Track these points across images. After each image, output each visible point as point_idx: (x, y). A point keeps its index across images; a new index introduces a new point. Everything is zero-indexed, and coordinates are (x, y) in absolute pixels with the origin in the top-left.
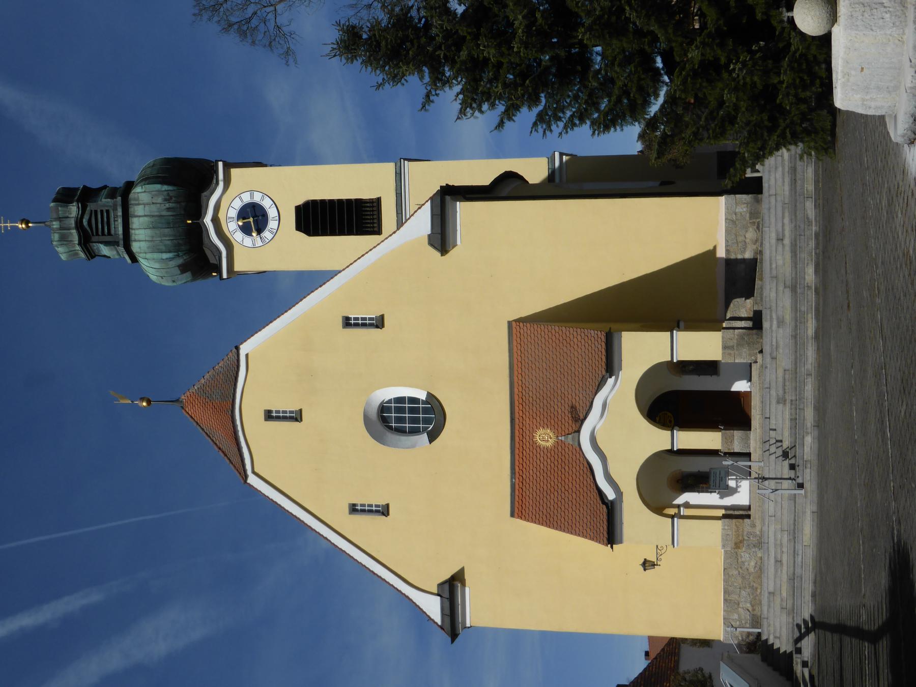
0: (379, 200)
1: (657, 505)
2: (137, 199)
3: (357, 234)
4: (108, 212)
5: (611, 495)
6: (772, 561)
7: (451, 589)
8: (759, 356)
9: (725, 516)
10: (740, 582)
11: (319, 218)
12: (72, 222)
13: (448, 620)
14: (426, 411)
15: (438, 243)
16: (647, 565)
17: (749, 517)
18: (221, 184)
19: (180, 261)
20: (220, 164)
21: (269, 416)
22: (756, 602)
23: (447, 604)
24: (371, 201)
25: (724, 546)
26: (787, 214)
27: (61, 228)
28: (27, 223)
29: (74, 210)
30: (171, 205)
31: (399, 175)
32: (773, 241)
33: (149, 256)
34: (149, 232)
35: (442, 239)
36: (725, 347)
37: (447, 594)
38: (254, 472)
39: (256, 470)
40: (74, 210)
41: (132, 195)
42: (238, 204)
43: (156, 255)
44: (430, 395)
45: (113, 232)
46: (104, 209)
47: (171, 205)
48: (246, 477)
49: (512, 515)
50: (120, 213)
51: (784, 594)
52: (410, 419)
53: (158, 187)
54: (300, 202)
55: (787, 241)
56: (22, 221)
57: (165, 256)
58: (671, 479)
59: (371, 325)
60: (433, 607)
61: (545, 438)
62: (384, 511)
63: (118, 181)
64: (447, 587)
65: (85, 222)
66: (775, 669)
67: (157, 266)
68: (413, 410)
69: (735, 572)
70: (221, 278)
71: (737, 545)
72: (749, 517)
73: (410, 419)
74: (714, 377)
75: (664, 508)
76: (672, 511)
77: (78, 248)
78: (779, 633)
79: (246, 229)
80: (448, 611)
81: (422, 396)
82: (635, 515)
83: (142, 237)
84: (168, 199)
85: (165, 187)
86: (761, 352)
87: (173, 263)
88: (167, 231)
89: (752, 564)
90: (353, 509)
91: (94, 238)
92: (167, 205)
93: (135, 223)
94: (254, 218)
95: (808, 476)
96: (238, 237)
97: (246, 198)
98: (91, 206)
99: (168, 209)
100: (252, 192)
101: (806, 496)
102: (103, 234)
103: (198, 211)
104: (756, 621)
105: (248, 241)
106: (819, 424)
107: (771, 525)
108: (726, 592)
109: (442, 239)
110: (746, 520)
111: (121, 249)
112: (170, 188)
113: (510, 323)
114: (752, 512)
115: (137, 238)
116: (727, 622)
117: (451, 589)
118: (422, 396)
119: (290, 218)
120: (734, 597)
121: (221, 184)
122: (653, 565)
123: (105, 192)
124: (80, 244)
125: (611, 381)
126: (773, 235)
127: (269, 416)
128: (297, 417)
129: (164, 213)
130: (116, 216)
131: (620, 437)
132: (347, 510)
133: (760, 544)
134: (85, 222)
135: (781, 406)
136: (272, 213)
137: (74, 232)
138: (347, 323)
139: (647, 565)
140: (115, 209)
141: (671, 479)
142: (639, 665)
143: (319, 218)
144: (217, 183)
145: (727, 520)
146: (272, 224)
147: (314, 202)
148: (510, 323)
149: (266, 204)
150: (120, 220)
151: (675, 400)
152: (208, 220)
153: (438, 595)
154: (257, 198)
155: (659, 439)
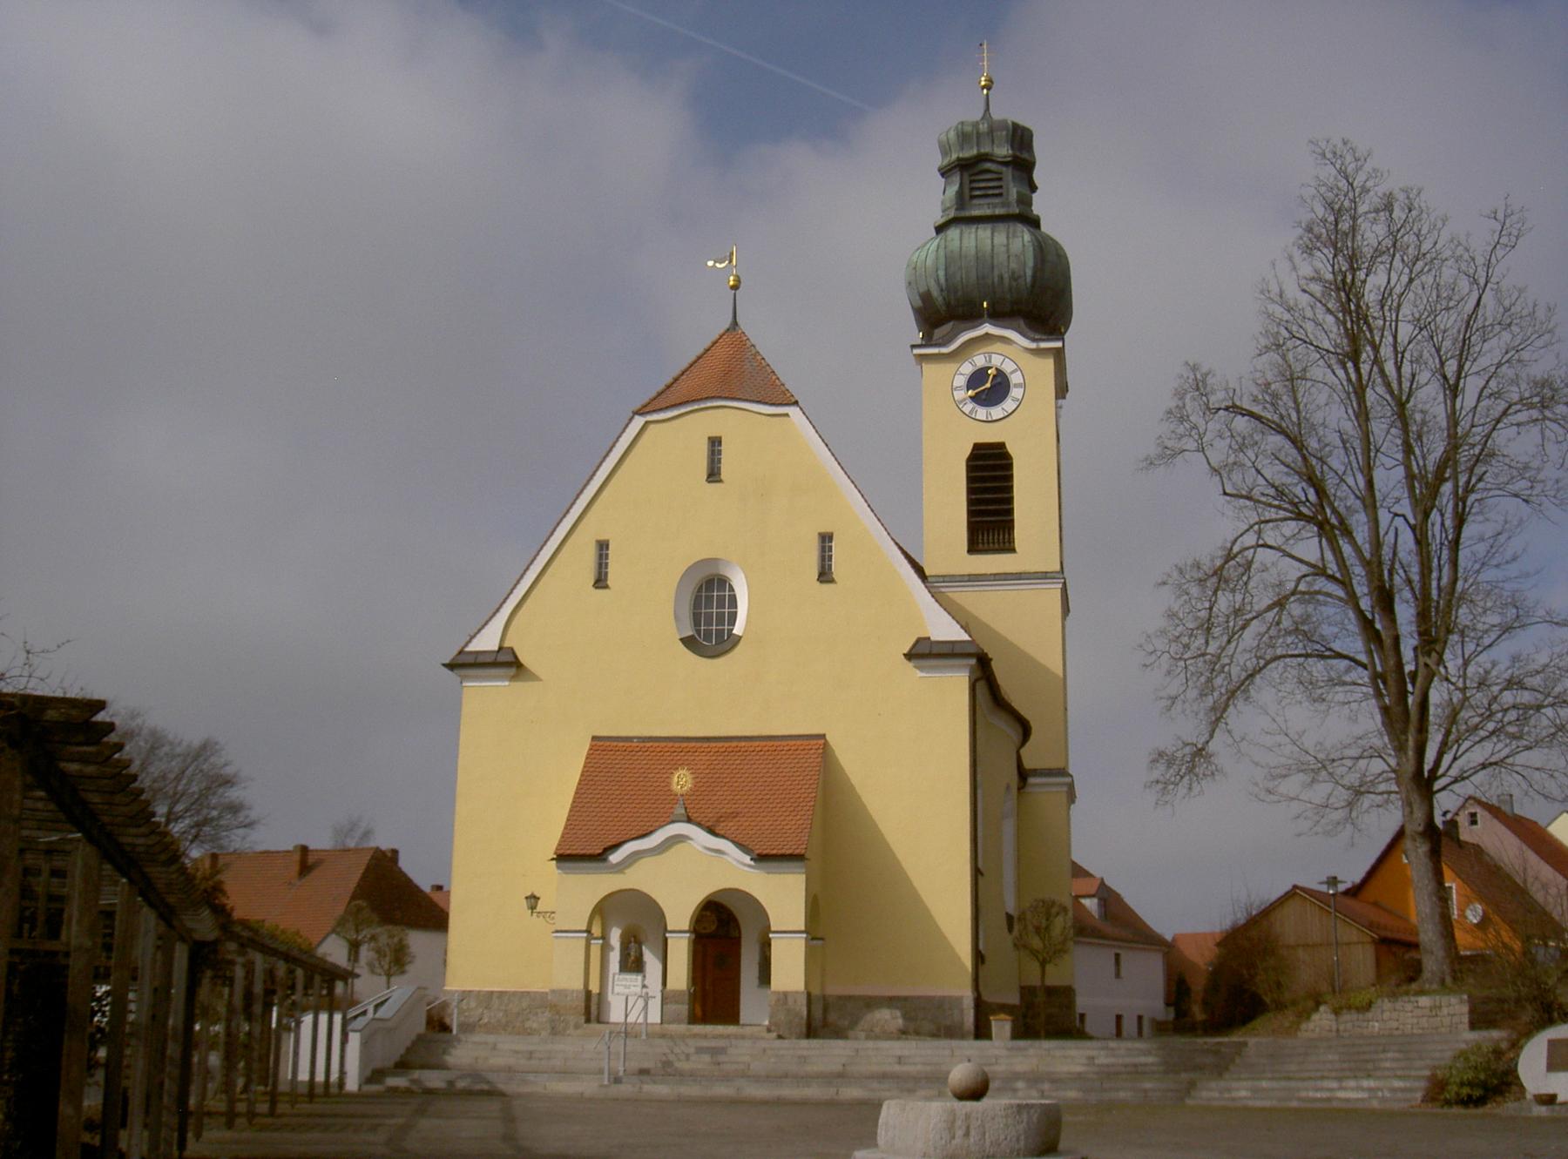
0: (1013, 550)
1: (604, 910)
2: (1014, 236)
3: (969, 523)
4: (1000, 195)
5: (615, 858)
6: (531, 1048)
7: (506, 663)
8: (774, 1035)
9: (588, 994)
10: (516, 1011)
11: (990, 474)
12: (986, 149)
13: (470, 659)
14: (720, 633)
15: (920, 650)
16: (533, 900)
17: (588, 1021)
18: (1033, 345)
19: (935, 293)
20: (1059, 344)
21: (715, 443)
22: (490, 1029)
23: (489, 659)
24: (1011, 540)
25: (553, 991)
26: (928, 1068)
27: (979, 135)
28: (988, 87)
29: (1003, 151)
30: (1006, 281)
31: (1044, 576)
32: (899, 1053)
33: (942, 253)
34: (973, 251)
35: (924, 653)
36: (786, 994)
37: (502, 658)
38: (647, 423)
39: (652, 426)
40: (1003, 151)
41: (1020, 227)
42: (1008, 367)
43: (942, 261)
44: (740, 638)
45: (976, 202)
46: (1003, 191)
47: (1006, 281)
48: (640, 412)
49: (594, 738)
50: (998, 211)
51: (492, 1061)
52: (708, 618)
53: (1030, 263)
54: (1010, 449)
55: (897, 1068)
56: (990, 82)
57: (941, 273)
58: (631, 926)
59: (823, 567)
60: (487, 641)
61: (682, 781)
62: (601, 582)
63: (1039, 206)
64: (510, 658)
65: (988, 165)
66: (408, 1050)
67: (929, 262)
68: (720, 617)
69: (524, 1005)
70: (913, 346)
71: (553, 1007)
72: (588, 1021)
73: (708, 618)
74: (756, 982)
75: (603, 919)
76: (596, 931)
77: (954, 156)
78: (463, 1054)
79: (977, 378)
80: (481, 659)
81: (737, 630)
82: (593, 886)
83: (965, 242)
84: (1014, 277)
85: (1029, 273)
86: (780, 1037)
87: (932, 284)
88: (973, 275)
89: (535, 1025)
90: (603, 546)
91: (966, 176)
92: (1006, 276)
93: (984, 232)
94: (990, 388)
95: (626, 1089)
96: (967, 369)
97: (1015, 379)
98: (1008, 173)
99: (1001, 277)
100: (1024, 385)
101: (602, 1086)
102: (972, 189)
103: (998, 315)
104: (467, 1028)
105: (961, 381)
106: (681, 1101)
107: (582, 1046)
108: (502, 993)
109: (924, 653)
110: (583, 1018)
111: (952, 214)
112: (1029, 279)
113: (823, 736)
114: (594, 1026)
115: (966, 235)
116: (465, 995)
117: (506, 663)
118: (737, 630)
119: (989, 435)
120: (495, 1002)
121: (1033, 345)
122: (533, 908)
123: (1026, 191)
124: (959, 159)
125: (747, 859)
126: (906, 1053)
127: (715, 443)
128: (714, 475)
129: (996, 273)
130: (995, 206)
131: (686, 869)
132: (602, 538)
133: (554, 1032)
134: (988, 165)
135: (1084, 1061)
136: (996, 412)
137: (974, 152)
138: (826, 539)
139: (533, 900)
140: (1003, 205)
141: (631, 926)
142: (425, 883)
143: (990, 474)
144: (1034, 340)
145: (582, 996)
146: (982, 413)
147: (1009, 467)
148: (823, 736)
149: (1008, 405)
150: (988, 212)
151: (723, 931)
152: (988, 328)
153: (500, 648)
154: (1016, 393)
155: (680, 913)
